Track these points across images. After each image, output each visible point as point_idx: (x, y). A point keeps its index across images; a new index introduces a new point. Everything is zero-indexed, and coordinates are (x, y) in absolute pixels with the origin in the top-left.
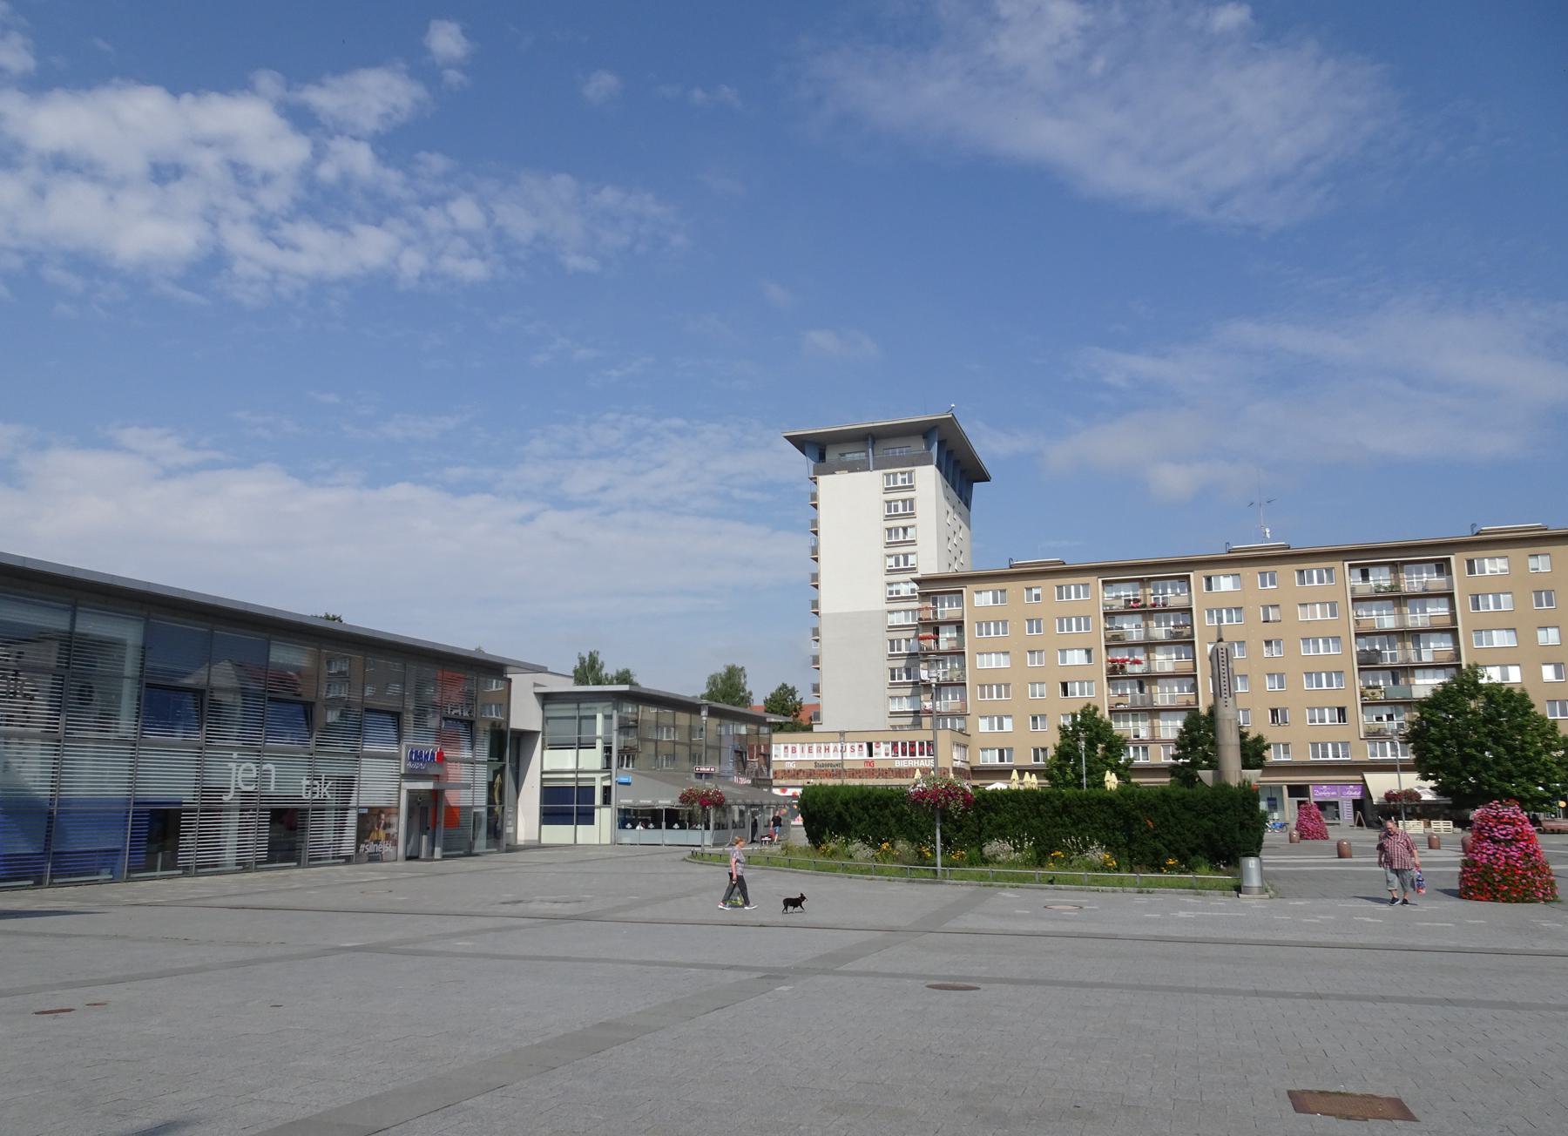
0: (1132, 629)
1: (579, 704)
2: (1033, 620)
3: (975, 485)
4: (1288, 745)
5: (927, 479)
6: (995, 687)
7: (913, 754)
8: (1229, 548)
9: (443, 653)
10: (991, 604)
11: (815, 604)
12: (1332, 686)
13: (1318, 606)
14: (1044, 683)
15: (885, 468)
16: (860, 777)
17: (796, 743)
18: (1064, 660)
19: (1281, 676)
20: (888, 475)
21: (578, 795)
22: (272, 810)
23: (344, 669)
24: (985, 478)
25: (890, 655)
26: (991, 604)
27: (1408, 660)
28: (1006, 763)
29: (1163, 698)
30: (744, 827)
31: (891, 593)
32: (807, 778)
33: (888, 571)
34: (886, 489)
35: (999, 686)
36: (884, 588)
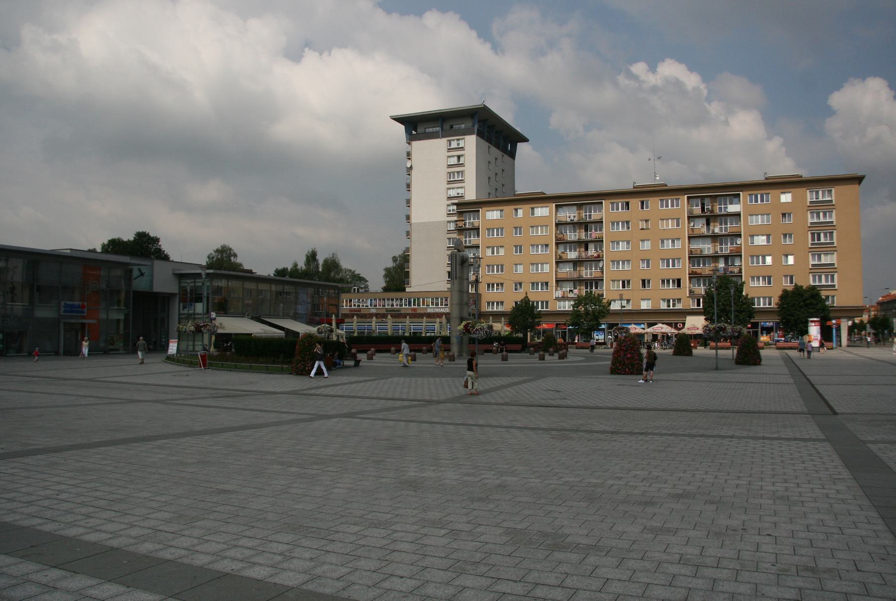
0: (571, 235)
2: (517, 227)
4: (834, 296)
5: (470, 142)
6: (760, 257)
7: (437, 304)
8: (766, 176)
9: (44, 252)
11: (408, 218)
12: (759, 264)
13: (760, 216)
14: (548, 263)
15: (448, 137)
19: (648, 261)
24: (524, 140)
25: (448, 247)
27: (717, 252)
29: (586, 274)
31: (450, 211)
32: (382, 318)
33: (448, 198)
34: (449, 149)
35: (498, 266)
36: (446, 208)
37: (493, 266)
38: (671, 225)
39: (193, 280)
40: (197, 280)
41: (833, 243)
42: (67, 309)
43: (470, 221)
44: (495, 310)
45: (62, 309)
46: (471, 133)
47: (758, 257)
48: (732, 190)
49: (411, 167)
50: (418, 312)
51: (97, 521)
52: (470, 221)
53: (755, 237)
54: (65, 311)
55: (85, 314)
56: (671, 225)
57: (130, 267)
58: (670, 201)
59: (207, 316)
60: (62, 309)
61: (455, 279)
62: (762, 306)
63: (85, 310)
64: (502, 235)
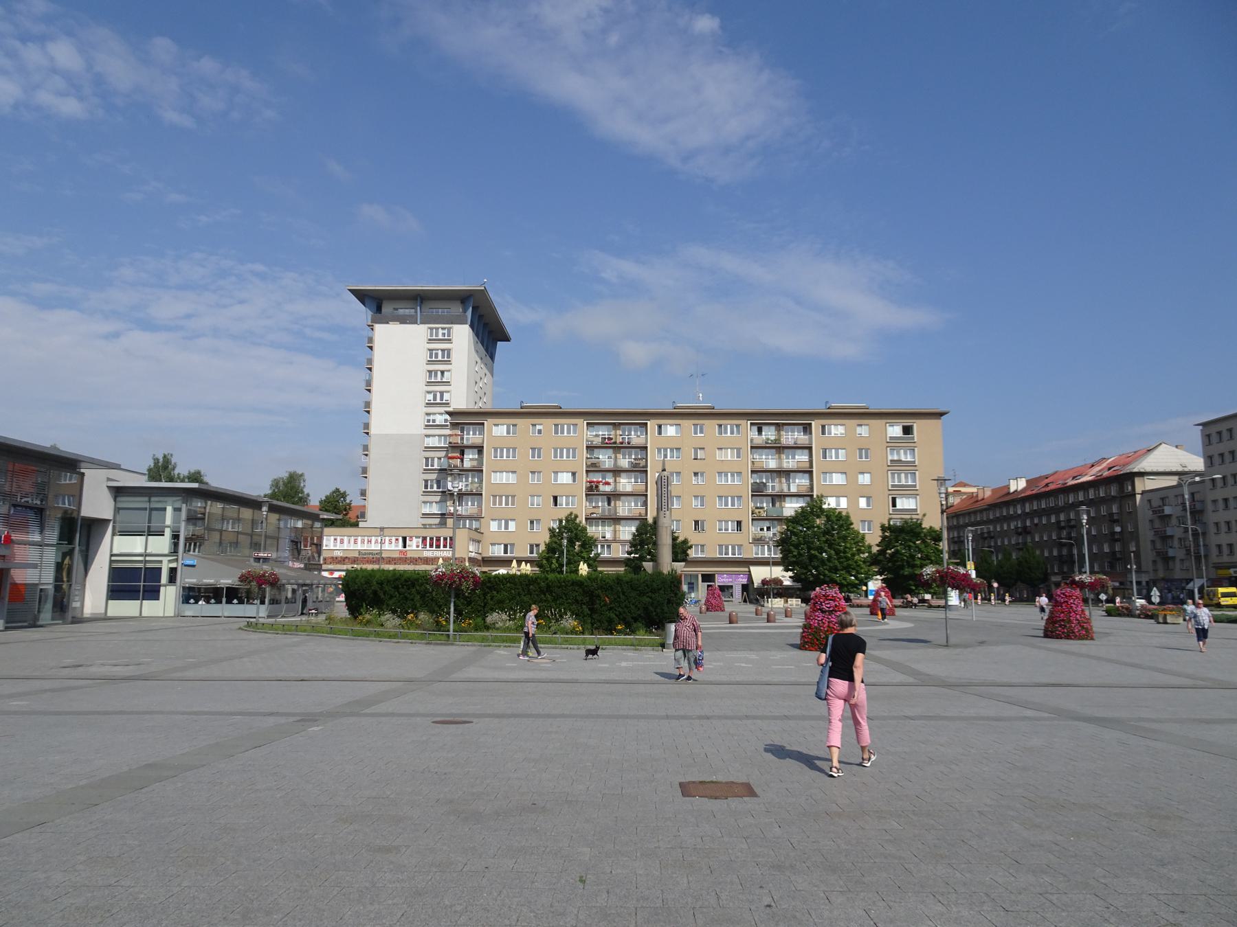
5: (462, 335)
7: (438, 546)
11: (367, 426)
19: (702, 497)
24: (506, 338)
25: (425, 470)
29: (624, 510)
31: (429, 421)
33: (427, 404)
35: (507, 497)
37: (726, 497)
38: (729, 455)
39: (147, 499)
40: (153, 499)
41: (915, 486)
46: (463, 322)
47: (501, 497)
48: (640, 418)
50: (408, 556)
52: (471, 437)
53: (559, 473)
56: (729, 455)
58: (729, 426)
62: (730, 556)
64: (514, 457)
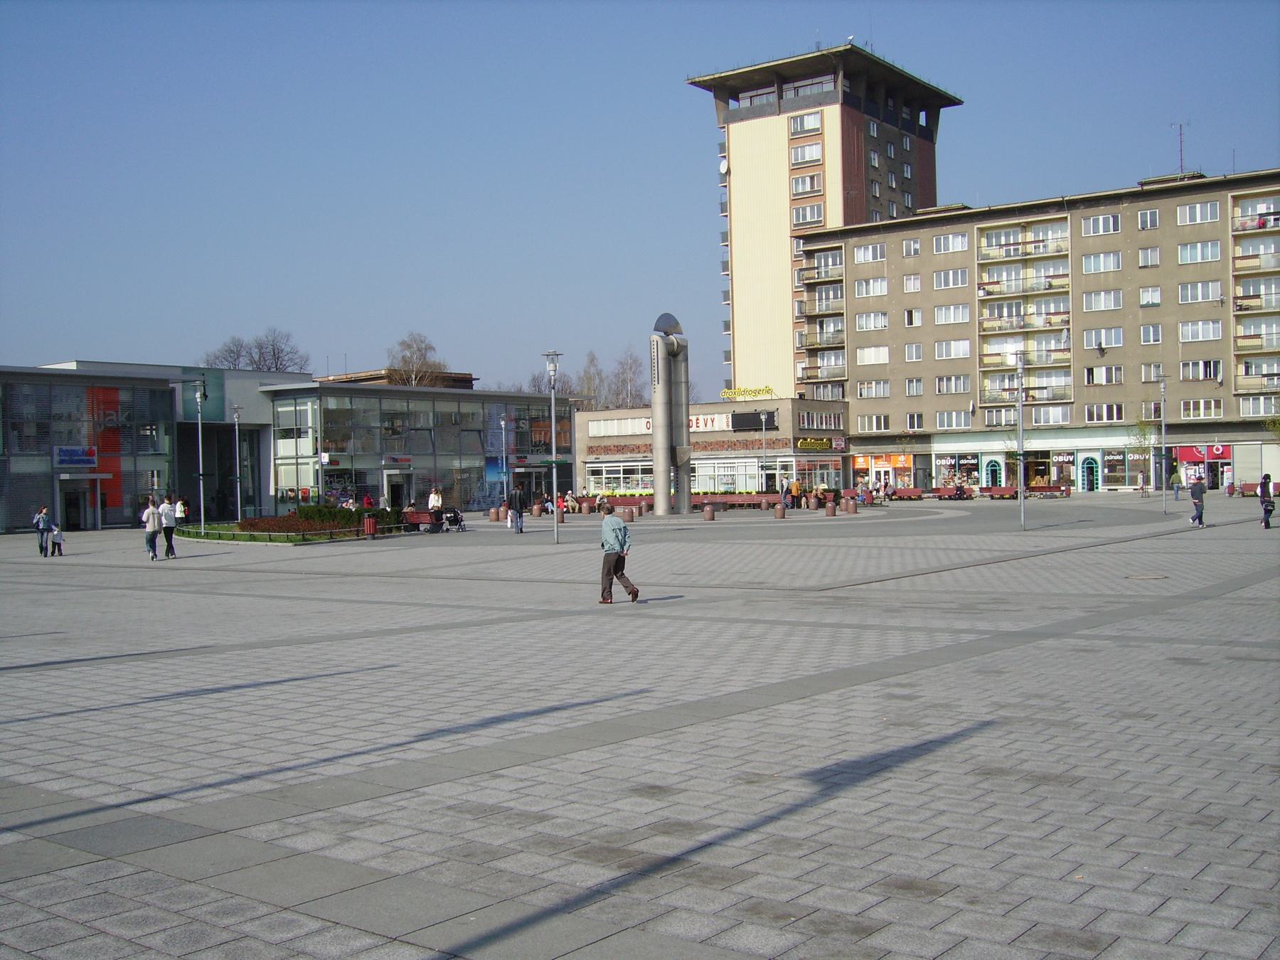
1: (295, 399)
3: (943, 111)
10: (871, 260)
16: (712, 450)
17: (714, 414)
18: (1089, 305)
20: (795, 118)
21: (1186, 442)
22: (254, 497)
23: (1238, 211)
24: (953, 102)
26: (871, 260)
28: (883, 430)
30: (1017, 497)
42: (63, 458)
43: (829, 268)
44: (1202, 417)
45: (56, 458)
49: (728, 172)
51: (1066, 857)
54: (62, 462)
55: (95, 465)
57: (171, 385)
59: (317, 459)
60: (56, 458)
61: (656, 382)
63: (95, 458)
